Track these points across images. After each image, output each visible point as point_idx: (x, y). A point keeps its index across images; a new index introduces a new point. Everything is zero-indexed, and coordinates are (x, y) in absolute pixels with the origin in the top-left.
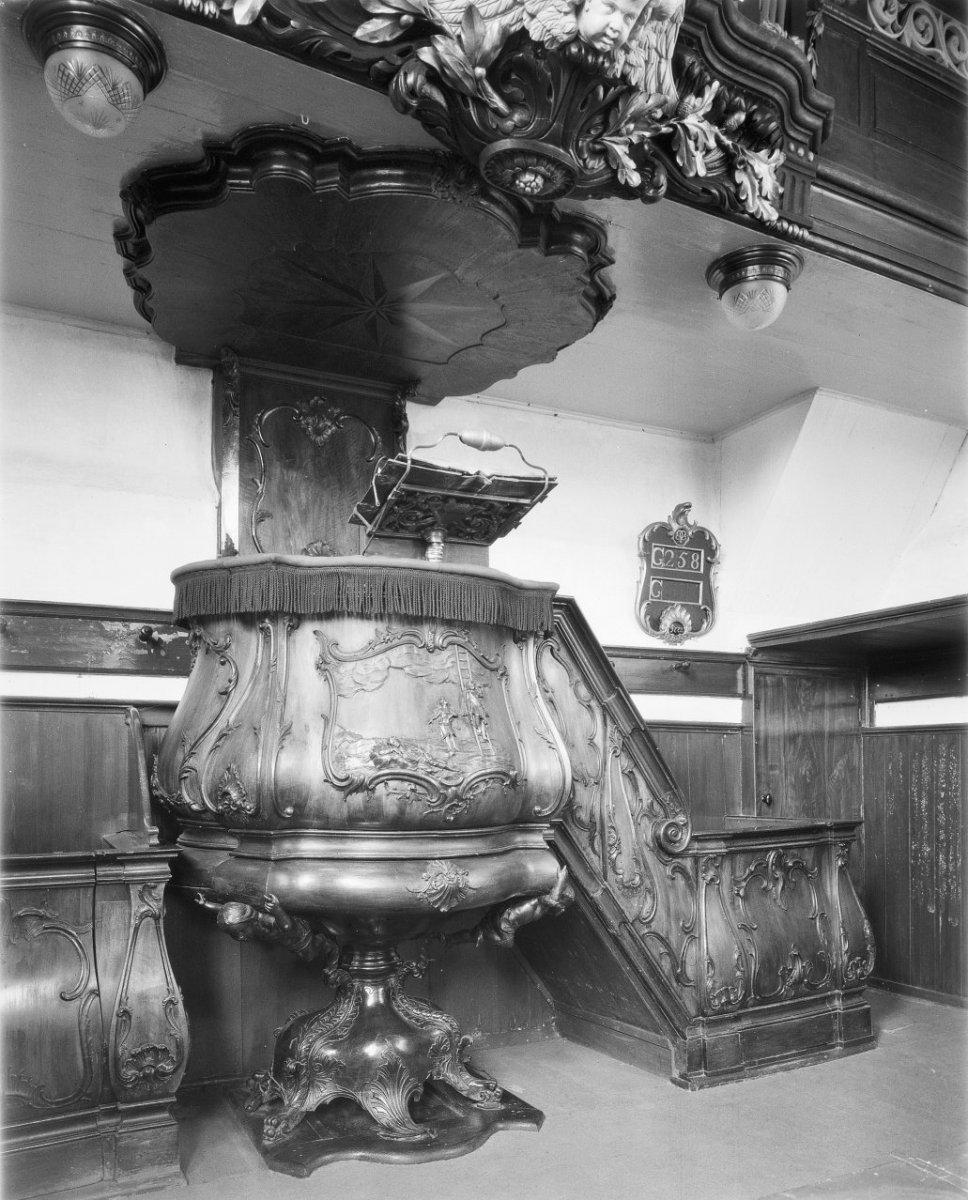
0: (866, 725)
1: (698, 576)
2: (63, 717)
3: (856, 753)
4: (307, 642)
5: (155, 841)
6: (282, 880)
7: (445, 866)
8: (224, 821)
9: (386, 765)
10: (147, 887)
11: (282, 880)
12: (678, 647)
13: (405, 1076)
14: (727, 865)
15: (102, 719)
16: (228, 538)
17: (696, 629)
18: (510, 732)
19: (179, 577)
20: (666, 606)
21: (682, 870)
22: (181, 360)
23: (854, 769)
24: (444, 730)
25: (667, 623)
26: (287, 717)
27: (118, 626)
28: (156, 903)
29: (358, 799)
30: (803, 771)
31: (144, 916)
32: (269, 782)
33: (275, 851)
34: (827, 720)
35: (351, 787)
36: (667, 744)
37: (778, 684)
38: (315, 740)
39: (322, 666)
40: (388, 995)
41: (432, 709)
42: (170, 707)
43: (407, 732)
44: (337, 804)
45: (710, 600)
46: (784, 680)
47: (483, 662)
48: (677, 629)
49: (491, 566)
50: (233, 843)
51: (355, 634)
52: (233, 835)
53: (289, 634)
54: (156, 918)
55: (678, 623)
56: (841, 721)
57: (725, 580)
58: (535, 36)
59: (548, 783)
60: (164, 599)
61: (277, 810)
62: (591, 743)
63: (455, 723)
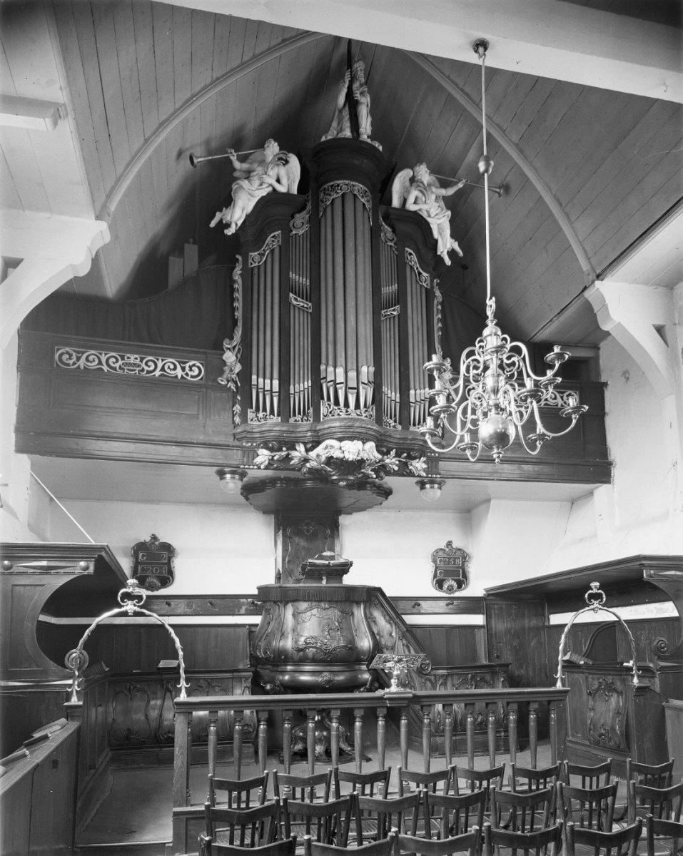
0: (547, 624)
1: (460, 567)
2: (401, 321)
3: (543, 636)
4: (290, 610)
5: (249, 666)
6: (281, 677)
7: (327, 674)
8: (266, 661)
9: (308, 644)
10: (246, 679)
11: (281, 677)
12: (452, 595)
13: (324, 743)
14: (449, 679)
15: (238, 630)
16: (279, 570)
17: (460, 587)
18: (352, 633)
19: (259, 588)
20: (444, 580)
21: (430, 681)
22: (264, 513)
23: (542, 643)
24: (326, 633)
25: (446, 586)
26: (284, 629)
27: (244, 600)
28: (249, 684)
29: (301, 653)
30: (515, 644)
31: (245, 687)
32: (277, 650)
33: (280, 669)
34: (526, 621)
35: (299, 650)
36: (418, 632)
37: (501, 608)
38: (290, 637)
39: (294, 615)
40: (322, 718)
41: (324, 626)
42: (257, 625)
43: (315, 634)
44: (297, 656)
45: (465, 576)
46: (504, 606)
47: (342, 612)
48: (450, 589)
49: (344, 583)
50: (270, 667)
51: (303, 606)
52: (271, 665)
53: (285, 607)
54: (249, 688)
55: (452, 586)
56: (534, 622)
57: (473, 569)
58: (335, 457)
59: (365, 649)
60: (256, 592)
61: (280, 657)
62: (391, 635)
63: (330, 631)
